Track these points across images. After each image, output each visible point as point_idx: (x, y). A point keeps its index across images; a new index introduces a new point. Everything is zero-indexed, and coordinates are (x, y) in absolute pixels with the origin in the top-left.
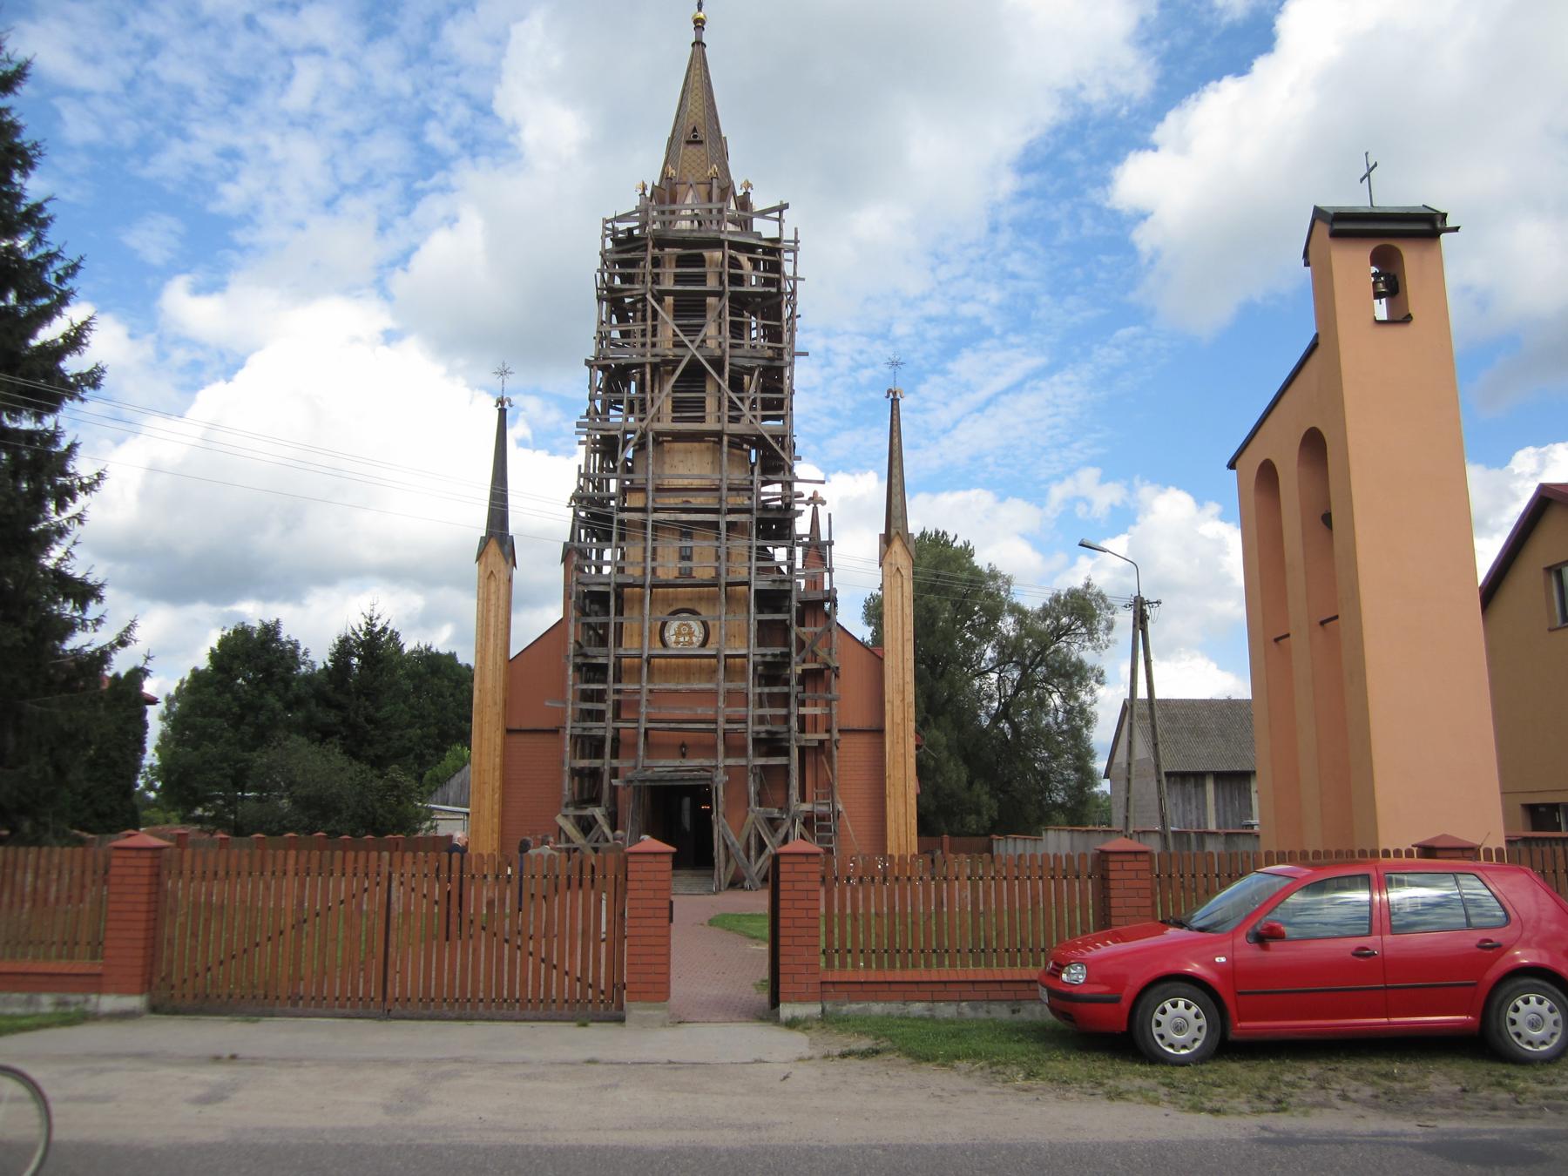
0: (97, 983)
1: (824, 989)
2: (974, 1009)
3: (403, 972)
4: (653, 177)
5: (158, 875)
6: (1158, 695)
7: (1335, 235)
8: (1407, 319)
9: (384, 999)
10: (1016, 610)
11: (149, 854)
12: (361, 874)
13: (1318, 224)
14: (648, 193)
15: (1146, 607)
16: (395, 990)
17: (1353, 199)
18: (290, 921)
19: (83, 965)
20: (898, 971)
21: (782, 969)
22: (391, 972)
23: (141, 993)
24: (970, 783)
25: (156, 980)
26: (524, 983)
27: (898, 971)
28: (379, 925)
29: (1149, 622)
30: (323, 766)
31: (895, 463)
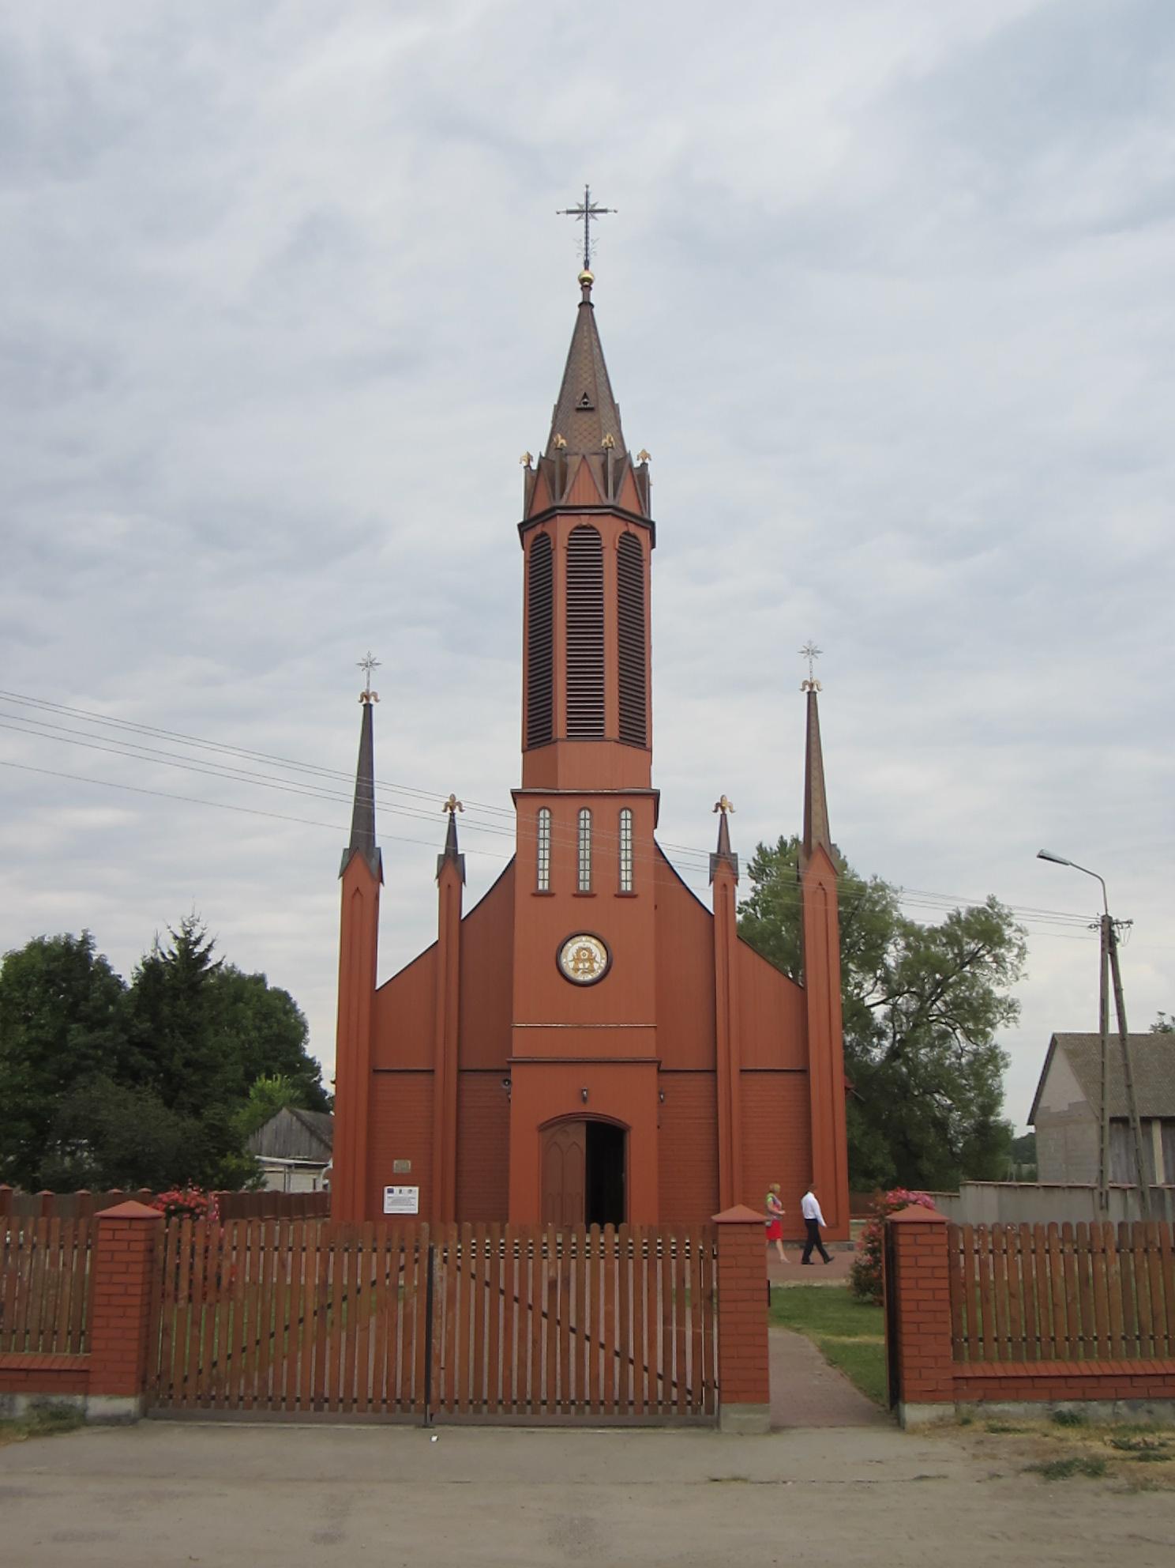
0: (83, 1381)
1: (959, 1388)
2: (1133, 1408)
3: (449, 1368)
5: (151, 1251)
6: (1131, 1029)
9: (428, 1401)
10: (909, 930)
11: (142, 1225)
14: (534, 466)
15: (1115, 928)
16: (439, 1390)
18: (312, 1306)
19: (63, 1358)
20: (1082, 1364)
22: (435, 1370)
23: (135, 1395)
24: (964, 1134)
27: (1082, 1364)
28: (417, 1305)
29: (1118, 946)
30: (142, 1115)
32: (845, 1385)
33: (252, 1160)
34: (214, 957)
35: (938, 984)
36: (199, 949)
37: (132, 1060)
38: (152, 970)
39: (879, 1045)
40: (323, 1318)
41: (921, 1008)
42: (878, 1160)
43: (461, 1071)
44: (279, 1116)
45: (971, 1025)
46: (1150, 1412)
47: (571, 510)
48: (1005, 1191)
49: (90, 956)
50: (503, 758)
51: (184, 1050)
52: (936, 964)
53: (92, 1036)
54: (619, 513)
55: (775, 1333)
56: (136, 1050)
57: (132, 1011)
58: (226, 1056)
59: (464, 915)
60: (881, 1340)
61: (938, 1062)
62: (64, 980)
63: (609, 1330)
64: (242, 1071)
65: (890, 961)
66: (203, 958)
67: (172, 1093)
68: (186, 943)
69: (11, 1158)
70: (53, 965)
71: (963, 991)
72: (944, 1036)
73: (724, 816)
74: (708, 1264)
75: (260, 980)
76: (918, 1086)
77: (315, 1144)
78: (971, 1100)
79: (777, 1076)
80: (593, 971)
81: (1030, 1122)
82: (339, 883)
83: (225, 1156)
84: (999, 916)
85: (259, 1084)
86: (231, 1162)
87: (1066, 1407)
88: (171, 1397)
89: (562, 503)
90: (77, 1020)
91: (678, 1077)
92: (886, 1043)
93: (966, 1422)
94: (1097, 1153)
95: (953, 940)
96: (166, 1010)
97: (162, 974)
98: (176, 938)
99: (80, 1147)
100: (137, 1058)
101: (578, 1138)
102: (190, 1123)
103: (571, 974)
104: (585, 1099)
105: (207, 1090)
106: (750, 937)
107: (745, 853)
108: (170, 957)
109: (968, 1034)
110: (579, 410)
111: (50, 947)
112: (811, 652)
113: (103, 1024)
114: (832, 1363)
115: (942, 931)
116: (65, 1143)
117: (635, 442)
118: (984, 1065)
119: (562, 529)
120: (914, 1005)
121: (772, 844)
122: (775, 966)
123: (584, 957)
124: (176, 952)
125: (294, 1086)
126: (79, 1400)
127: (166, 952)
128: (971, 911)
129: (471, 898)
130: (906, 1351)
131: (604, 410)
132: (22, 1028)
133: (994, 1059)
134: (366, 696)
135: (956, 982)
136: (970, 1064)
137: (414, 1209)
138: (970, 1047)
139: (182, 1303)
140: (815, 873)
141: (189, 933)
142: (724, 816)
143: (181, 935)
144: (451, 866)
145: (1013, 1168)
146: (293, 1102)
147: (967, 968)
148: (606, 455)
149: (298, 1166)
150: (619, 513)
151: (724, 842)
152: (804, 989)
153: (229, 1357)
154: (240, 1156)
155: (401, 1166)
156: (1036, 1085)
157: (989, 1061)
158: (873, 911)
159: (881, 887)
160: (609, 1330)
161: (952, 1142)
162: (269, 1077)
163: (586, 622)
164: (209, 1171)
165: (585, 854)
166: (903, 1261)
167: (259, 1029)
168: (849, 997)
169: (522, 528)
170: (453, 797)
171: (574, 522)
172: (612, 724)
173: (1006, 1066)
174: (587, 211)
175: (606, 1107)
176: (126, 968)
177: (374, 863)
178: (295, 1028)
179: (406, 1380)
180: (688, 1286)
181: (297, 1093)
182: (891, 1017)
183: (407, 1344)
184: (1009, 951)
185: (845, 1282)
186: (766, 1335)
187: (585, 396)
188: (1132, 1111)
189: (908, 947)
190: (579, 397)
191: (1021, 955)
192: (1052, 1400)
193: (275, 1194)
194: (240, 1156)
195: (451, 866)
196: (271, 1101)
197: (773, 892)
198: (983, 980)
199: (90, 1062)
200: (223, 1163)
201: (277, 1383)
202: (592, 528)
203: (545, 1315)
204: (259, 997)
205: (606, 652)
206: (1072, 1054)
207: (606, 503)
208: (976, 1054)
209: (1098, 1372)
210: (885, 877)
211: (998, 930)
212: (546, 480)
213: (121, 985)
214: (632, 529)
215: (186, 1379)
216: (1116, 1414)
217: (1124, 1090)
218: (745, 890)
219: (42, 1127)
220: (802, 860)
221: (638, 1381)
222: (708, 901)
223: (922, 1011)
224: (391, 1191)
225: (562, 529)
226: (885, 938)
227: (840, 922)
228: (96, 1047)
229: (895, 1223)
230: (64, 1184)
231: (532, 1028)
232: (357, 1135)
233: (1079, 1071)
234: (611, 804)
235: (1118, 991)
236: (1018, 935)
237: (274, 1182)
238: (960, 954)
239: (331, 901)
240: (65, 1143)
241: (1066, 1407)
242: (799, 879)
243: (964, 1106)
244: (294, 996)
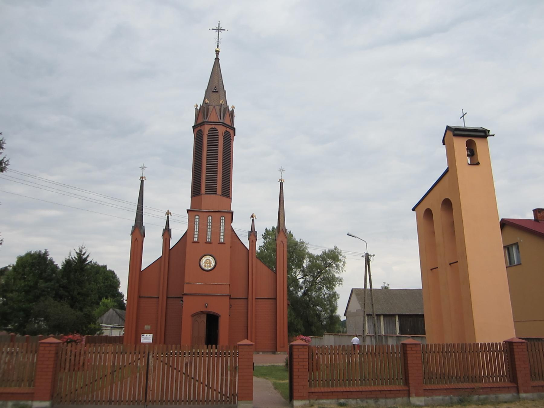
1: (310, 395)
2: (362, 401)
3: (153, 390)
4: (200, 103)
5: (57, 353)
6: (373, 288)
7: (455, 135)
8: (478, 164)
9: (146, 401)
10: (310, 256)
11: (54, 345)
12: (137, 353)
13: (448, 132)
14: (198, 108)
16: (150, 397)
17: (460, 124)
18: (109, 371)
19: (25, 389)
20: (347, 388)
21: (295, 388)
24: (325, 319)
25: (55, 395)
26: (199, 394)
27: (347, 388)
28: (143, 373)
29: (370, 262)
30: (63, 310)
31: (281, 205)
32: (279, 395)
33: (99, 325)
34: (89, 260)
35: (319, 272)
36: (84, 257)
38: (68, 263)
39: (301, 291)
40: (113, 374)
41: (313, 280)
42: (299, 327)
43: (167, 297)
44: (109, 311)
45: (328, 285)
46: (367, 402)
47: (209, 123)
49: (47, 258)
50: (183, 198)
52: (318, 267)
53: (47, 284)
54: (224, 125)
55: (255, 379)
56: (62, 289)
57: (61, 276)
58: (92, 291)
60: (287, 381)
61: (318, 296)
62: (37, 266)
63: (204, 378)
64: (97, 296)
65: (305, 265)
66: (86, 259)
68: (80, 255)
69: (16, 324)
70: (34, 261)
71: (326, 275)
72: (320, 289)
73: (253, 219)
74: (235, 357)
75: (105, 267)
76: (312, 304)
77: (121, 320)
78: (328, 308)
79: (268, 300)
80: (210, 266)
81: (345, 315)
84: (338, 252)
85: (103, 301)
86: (92, 326)
87: (342, 401)
88: (61, 401)
89: (207, 120)
90: (41, 279)
91: (237, 300)
92: (303, 291)
93: (312, 406)
94: (362, 325)
95: (324, 259)
96: (72, 276)
97: (71, 265)
98: (77, 253)
99: (40, 321)
100: (62, 292)
101: (204, 319)
102: (79, 313)
103: (204, 267)
104: (206, 307)
106: (261, 257)
107: (260, 231)
108: (74, 259)
109: (327, 288)
110: (213, 92)
111: (33, 254)
112: (282, 170)
113: (50, 280)
114: (276, 388)
116: (36, 319)
118: (332, 298)
119: (206, 129)
120: (311, 279)
121: (270, 229)
122: (269, 267)
123: (207, 262)
125: (115, 301)
126: (30, 403)
127: (73, 257)
128: (329, 251)
129: (173, 243)
130: (295, 384)
131: (221, 92)
132: (23, 281)
133: (335, 296)
134: (142, 178)
136: (328, 297)
137: (151, 341)
138: (328, 292)
139: (67, 370)
140: (281, 238)
141: (81, 251)
142: (253, 219)
143: (78, 252)
145: (341, 329)
146: (114, 307)
149: (115, 327)
150: (224, 125)
152: (276, 273)
153: (81, 388)
157: (333, 297)
158: (300, 250)
159: (302, 243)
160: (204, 378)
161: (322, 322)
162: (106, 298)
163: (212, 157)
164: (85, 329)
165: (209, 230)
166: (294, 357)
167: (104, 283)
168: (292, 276)
170: (168, 211)
171: (210, 126)
173: (339, 298)
174: (219, 30)
175: (213, 309)
176: (59, 262)
177: (142, 231)
178: (116, 283)
179: (139, 394)
180: (229, 365)
181: (116, 304)
182: (304, 282)
183: (140, 383)
184: (340, 263)
185: (284, 364)
186: (252, 379)
188: (373, 312)
189: (310, 261)
190: (213, 88)
192: (338, 399)
193: (107, 336)
194: (95, 324)
196: (107, 306)
197: (270, 244)
198: (332, 272)
200: (89, 326)
201: (97, 396)
203: (184, 374)
204: (104, 272)
206: (357, 295)
208: (330, 294)
209: (352, 390)
210: (304, 240)
211: (337, 257)
212: (202, 113)
213: (57, 268)
214: (228, 130)
215: (66, 395)
216: (357, 403)
217: (371, 305)
218: (260, 242)
219: (27, 314)
220: (277, 234)
221: (213, 394)
222: (247, 246)
223: (314, 281)
225: (206, 129)
226: (303, 258)
227: (289, 252)
228: (48, 288)
229: (293, 345)
230: (34, 333)
231: (191, 283)
232: (133, 317)
233: (359, 300)
234: (217, 214)
235: (370, 276)
237: (106, 333)
238: (326, 264)
239: (128, 242)
240: (36, 319)
241: (342, 401)
242: (275, 240)
243: (326, 310)
244: (116, 272)
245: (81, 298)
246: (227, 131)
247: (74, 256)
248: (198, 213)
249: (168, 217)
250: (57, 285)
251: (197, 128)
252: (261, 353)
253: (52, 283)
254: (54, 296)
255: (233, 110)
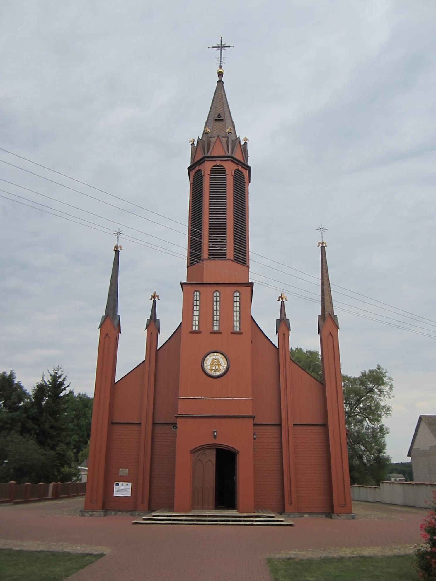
33: (76, 469)
37: (28, 425)
38: (41, 390)
43: (154, 424)
48: (406, 486)
51: (50, 422)
52: (357, 393)
54: (235, 160)
56: (30, 421)
59: (158, 348)
66: (61, 384)
67: (43, 439)
72: (361, 421)
73: (283, 302)
80: (220, 370)
82: (99, 331)
83: (64, 467)
84: (382, 373)
89: (208, 155)
98: (51, 375)
100: (30, 424)
101: (212, 457)
102: (52, 453)
103: (209, 372)
105: (60, 439)
108: (48, 383)
110: (216, 120)
112: (322, 229)
115: (359, 378)
117: (241, 133)
119: (207, 167)
123: (215, 363)
124: (50, 381)
129: (162, 339)
131: (228, 121)
134: (116, 247)
135: (364, 399)
136: (372, 432)
142: (283, 302)
143: (53, 374)
144: (153, 325)
147: (369, 394)
148: (228, 138)
150: (235, 160)
151: (283, 314)
152: (323, 384)
154: (70, 467)
155: (124, 471)
156: (412, 439)
163: (218, 209)
164: (56, 473)
169: (190, 169)
170: (155, 293)
171: (214, 163)
172: (230, 252)
174: (221, 47)
175: (226, 441)
177: (116, 322)
187: (219, 115)
191: (391, 388)
194: (70, 467)
195: (153, 325)
199: (9, 426)
200: (62, 470)
202: (222, 166)
205: (228, 220)
207: (228, 155)
214: (240, 168)
222: (275, 339)
224: (117, 485)
236: (389, 381)
238: (366, 388)
239: (94, 335)
243: (369, 449)
245: (54, 433)
246: (238, 170)
247: (48, 379)
248: (198, 288)
249: (154, 301)
250: (25, 415)
251: (195, 171)
252: (306, 516)
253: (18, 413)
254: (19, 429)
255: (246, 143)
